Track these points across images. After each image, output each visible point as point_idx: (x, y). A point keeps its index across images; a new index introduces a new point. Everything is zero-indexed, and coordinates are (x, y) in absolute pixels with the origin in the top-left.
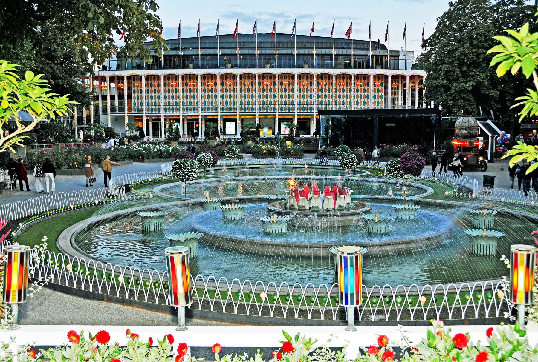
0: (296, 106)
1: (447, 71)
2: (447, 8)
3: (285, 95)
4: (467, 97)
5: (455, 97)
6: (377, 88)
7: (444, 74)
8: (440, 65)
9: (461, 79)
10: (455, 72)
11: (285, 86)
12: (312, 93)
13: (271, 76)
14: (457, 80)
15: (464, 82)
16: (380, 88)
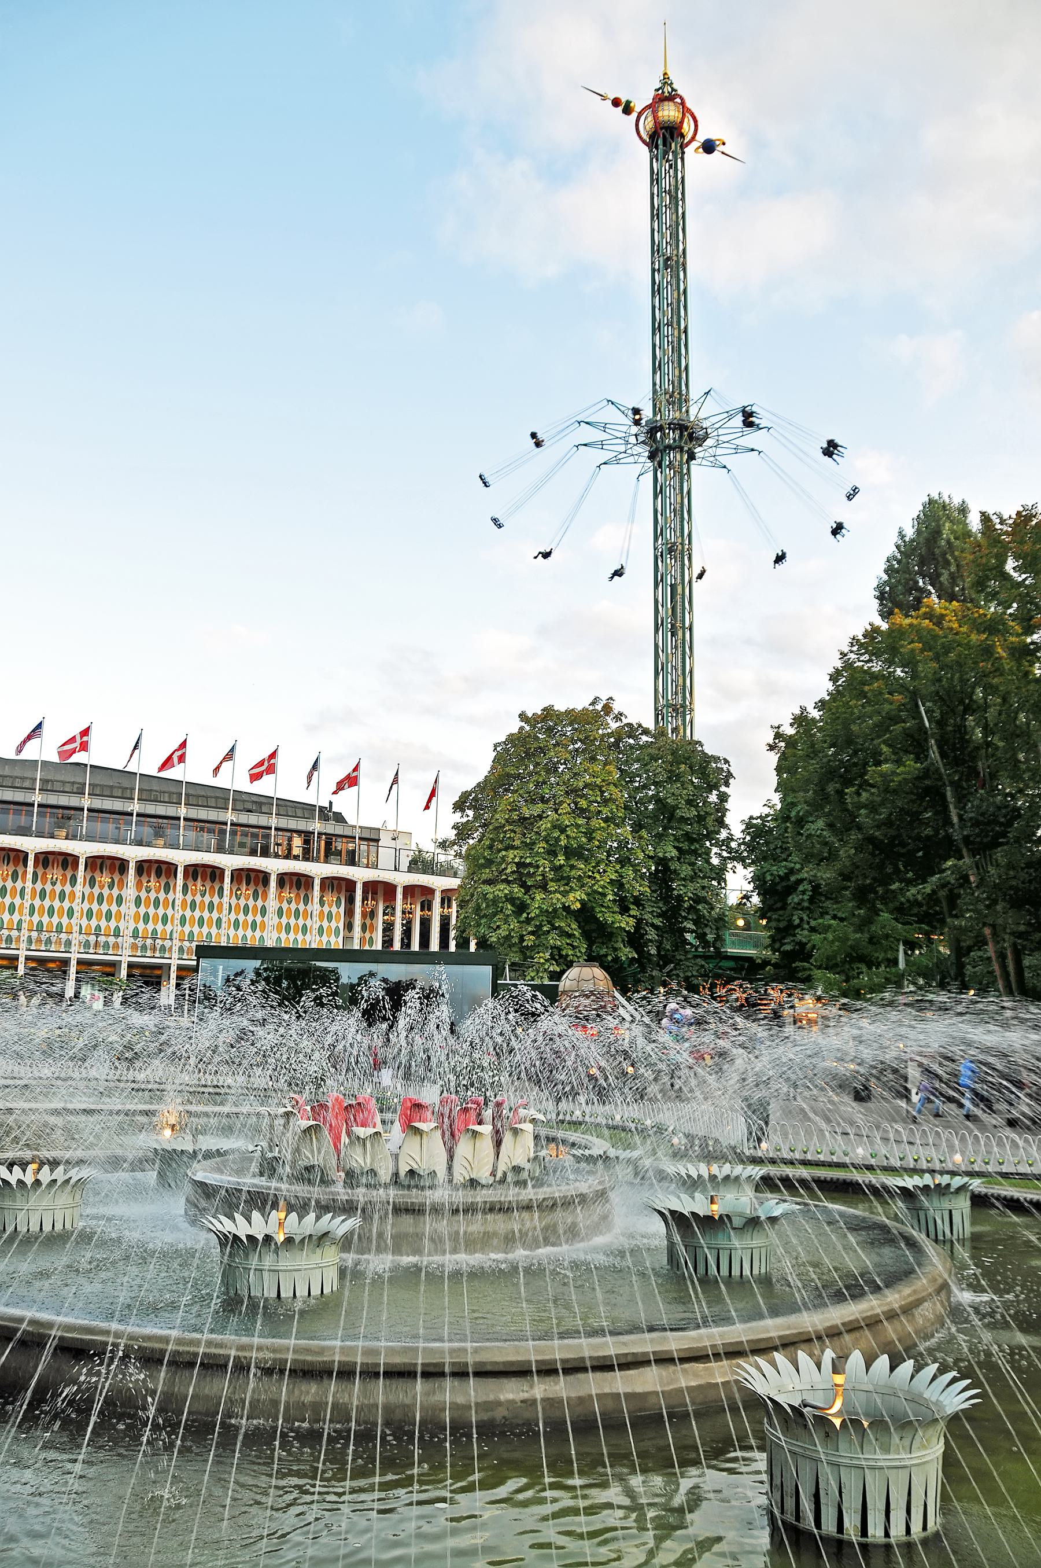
0: (127, 941)
1: (519, 865)
2: (514, 726)
3: (100, 911)
4: (567, 929)
5: (540, 926)
6: (326, 909)
7: (513, 872)
8: (500, 851)
9: (552, 884)
10: (538, 867)
11: (102, 887)
12: (309, 923)
13: (68, 861)
14: (543, 887)
15: (562, 893)
16: (334, 910)
